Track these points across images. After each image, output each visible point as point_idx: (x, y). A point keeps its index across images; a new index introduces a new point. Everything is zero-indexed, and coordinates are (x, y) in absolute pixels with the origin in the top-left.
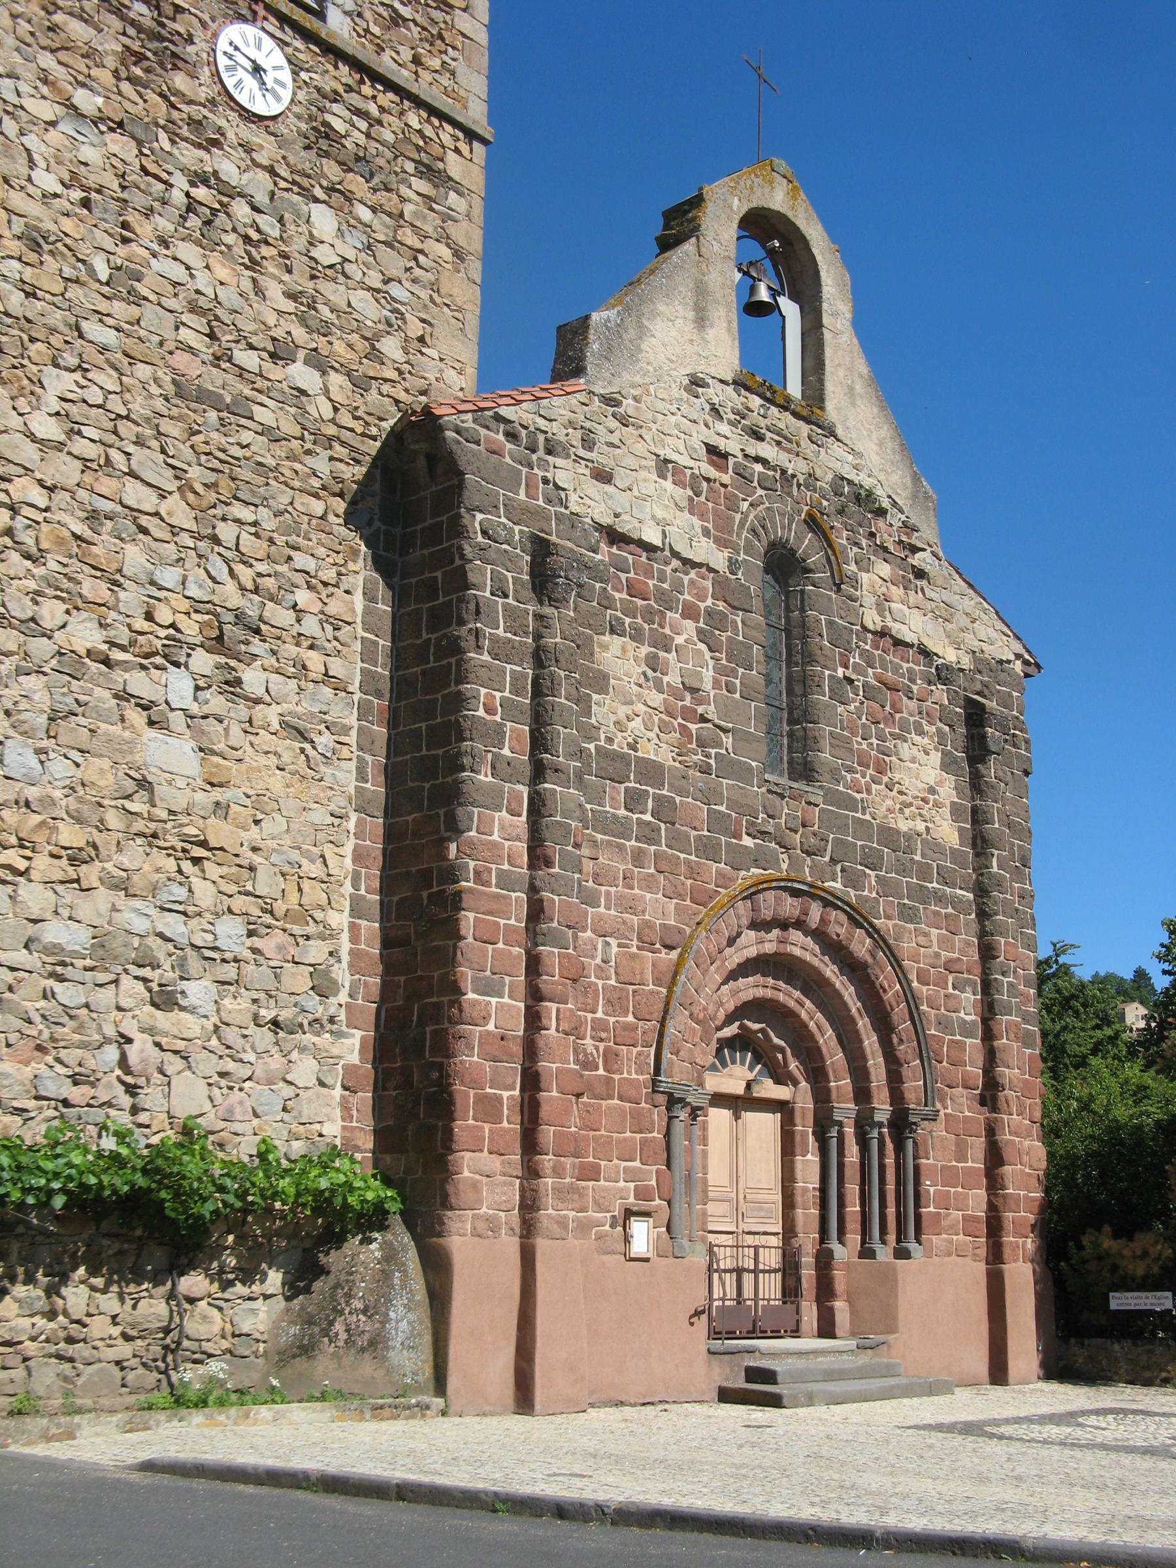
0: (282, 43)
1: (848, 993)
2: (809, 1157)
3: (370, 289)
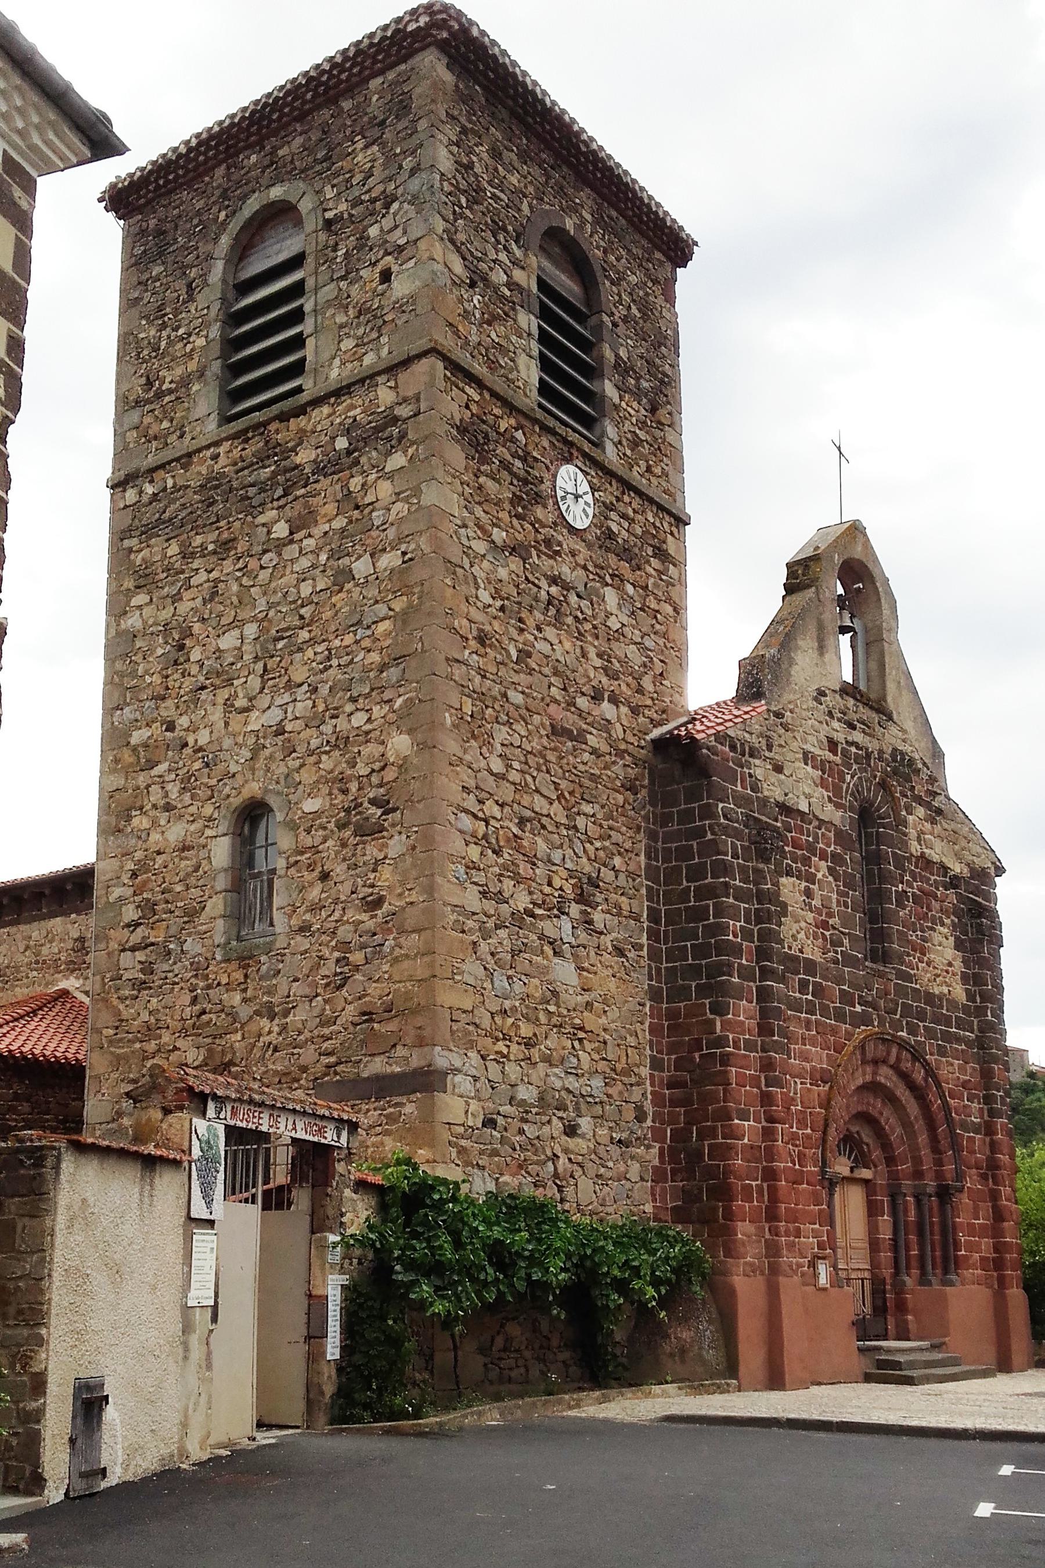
0: (586, 473)
1: (913, 1108)
2: (886, 1217)
3: (636, 643)
